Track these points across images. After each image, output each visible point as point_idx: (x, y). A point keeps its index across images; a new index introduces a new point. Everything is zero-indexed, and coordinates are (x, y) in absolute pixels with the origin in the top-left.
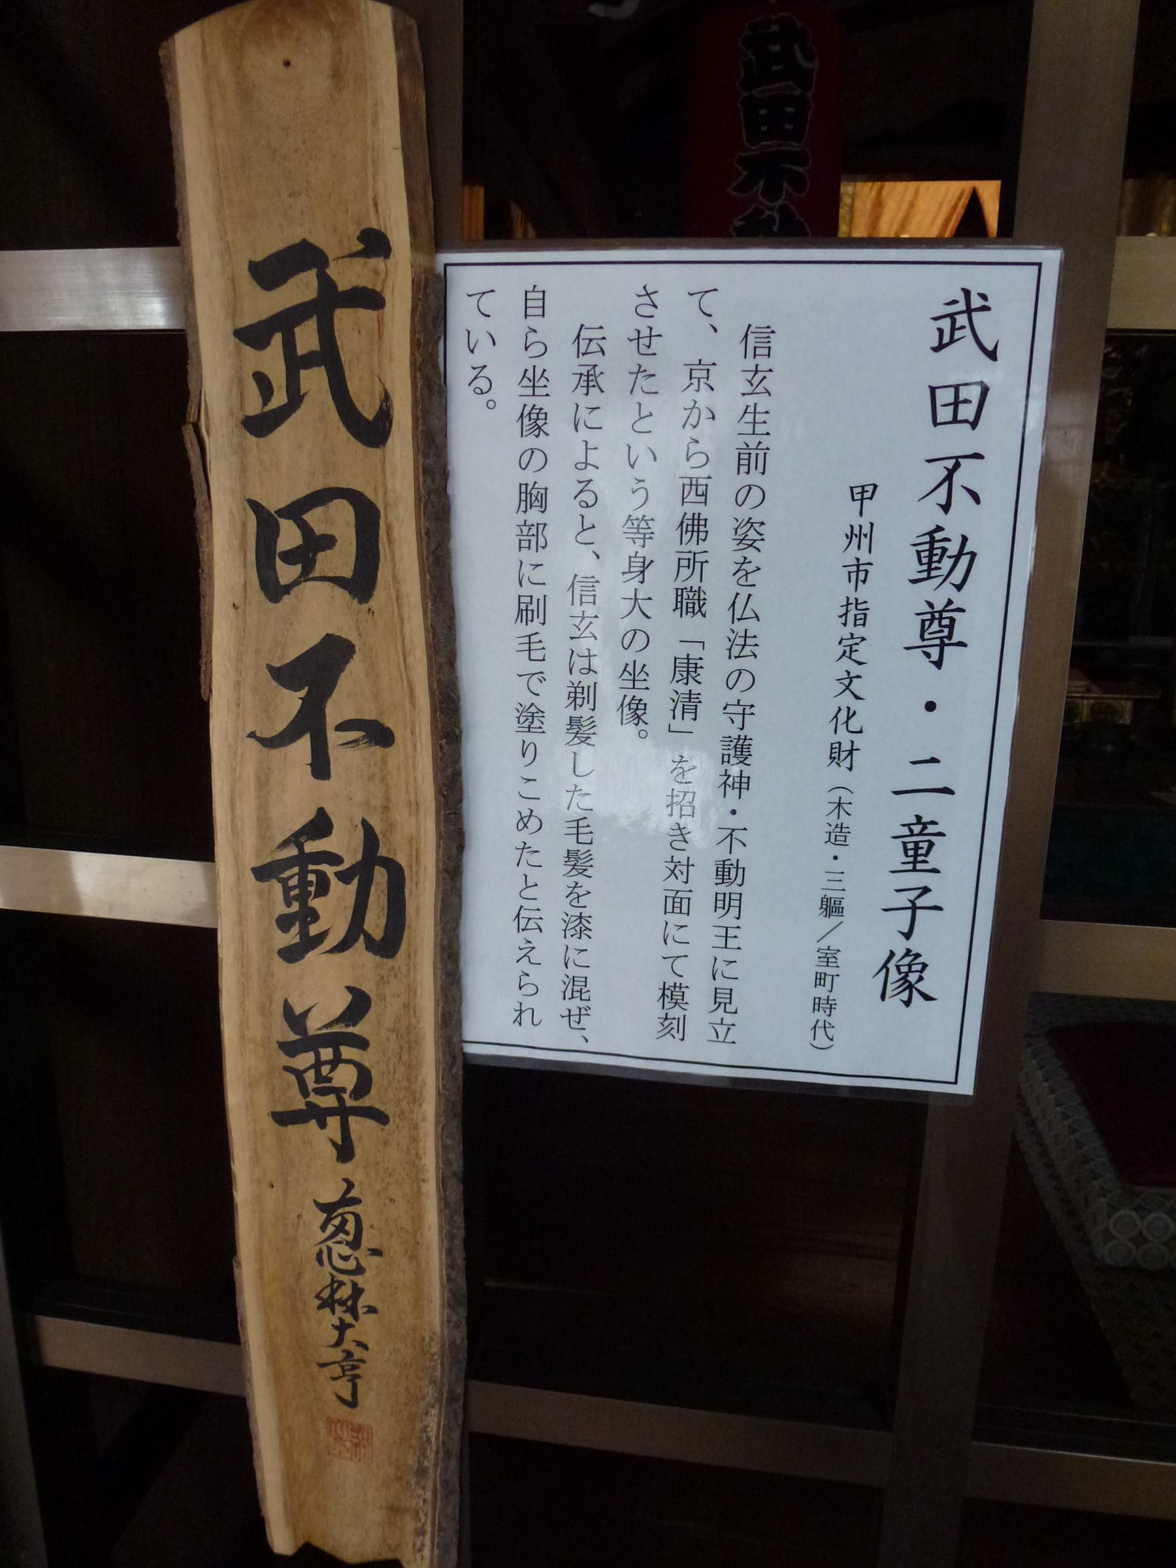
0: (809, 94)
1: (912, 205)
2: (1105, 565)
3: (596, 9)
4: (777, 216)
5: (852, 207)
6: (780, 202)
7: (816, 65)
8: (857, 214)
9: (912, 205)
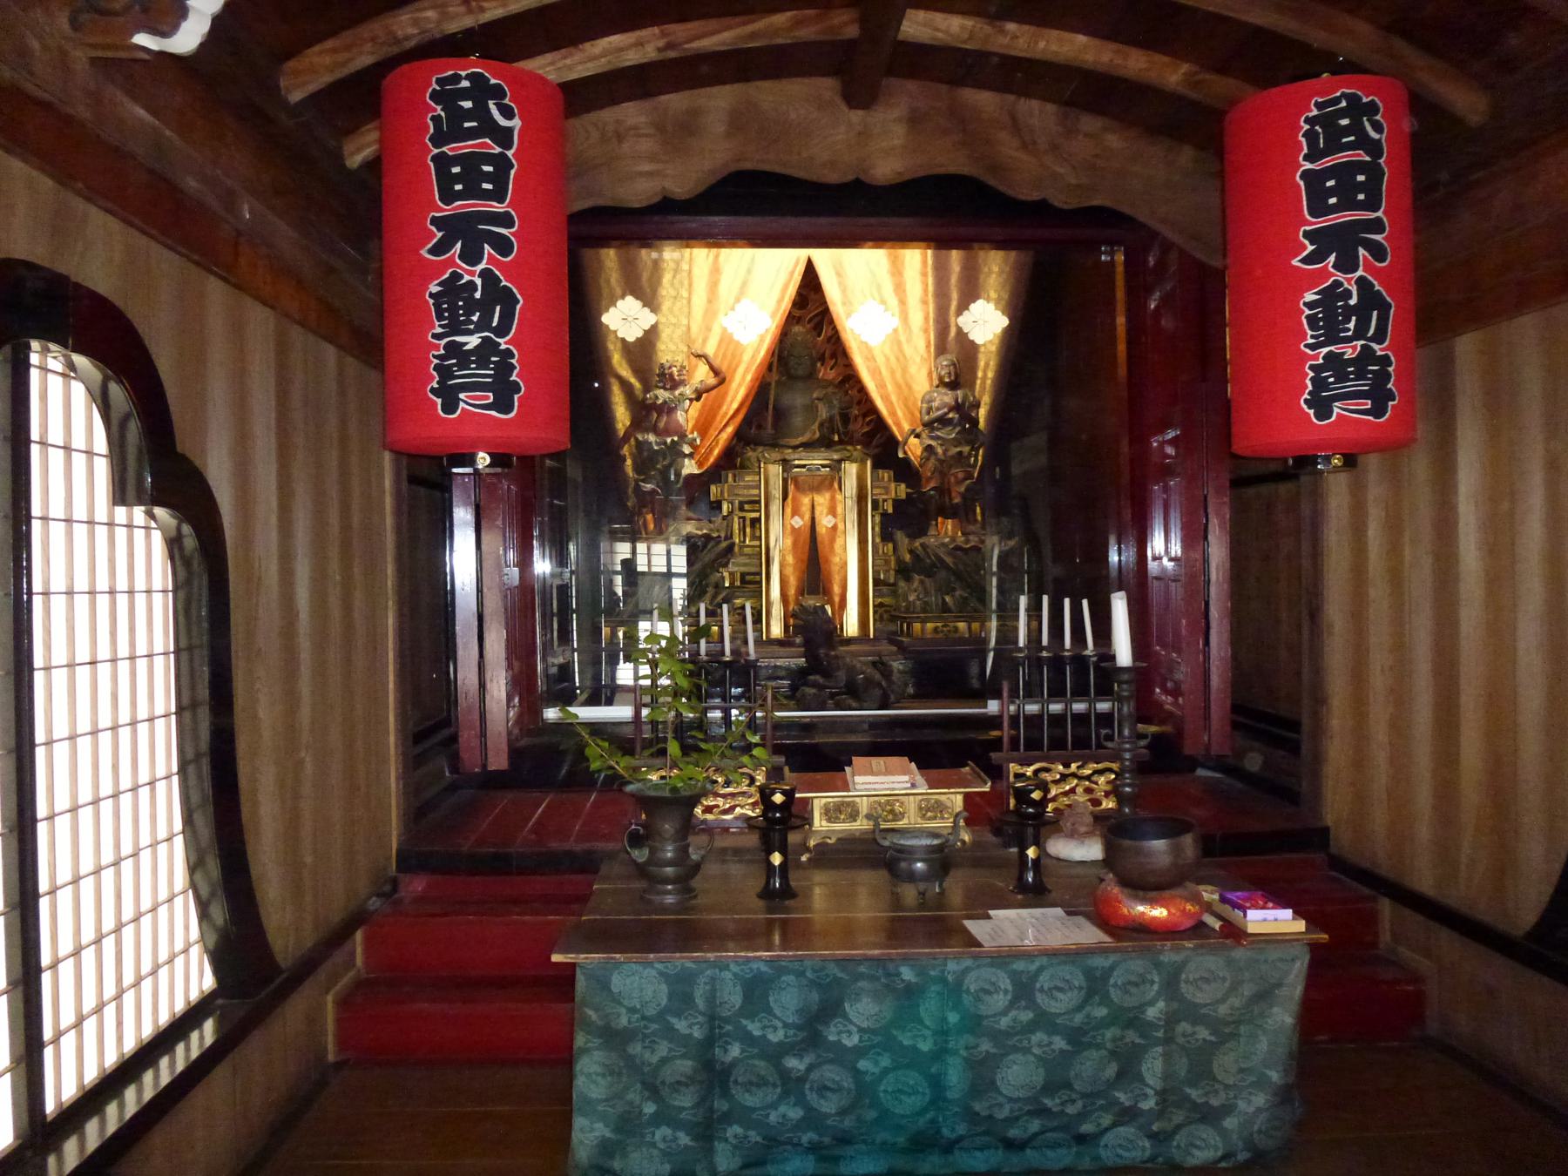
1: (749, 271)
2: (962, 625)
3: (142, 39)
4: (478, 282)
5: (690, 272)
7: (516, 123)
8: (695, 279)
9: (749, 271)
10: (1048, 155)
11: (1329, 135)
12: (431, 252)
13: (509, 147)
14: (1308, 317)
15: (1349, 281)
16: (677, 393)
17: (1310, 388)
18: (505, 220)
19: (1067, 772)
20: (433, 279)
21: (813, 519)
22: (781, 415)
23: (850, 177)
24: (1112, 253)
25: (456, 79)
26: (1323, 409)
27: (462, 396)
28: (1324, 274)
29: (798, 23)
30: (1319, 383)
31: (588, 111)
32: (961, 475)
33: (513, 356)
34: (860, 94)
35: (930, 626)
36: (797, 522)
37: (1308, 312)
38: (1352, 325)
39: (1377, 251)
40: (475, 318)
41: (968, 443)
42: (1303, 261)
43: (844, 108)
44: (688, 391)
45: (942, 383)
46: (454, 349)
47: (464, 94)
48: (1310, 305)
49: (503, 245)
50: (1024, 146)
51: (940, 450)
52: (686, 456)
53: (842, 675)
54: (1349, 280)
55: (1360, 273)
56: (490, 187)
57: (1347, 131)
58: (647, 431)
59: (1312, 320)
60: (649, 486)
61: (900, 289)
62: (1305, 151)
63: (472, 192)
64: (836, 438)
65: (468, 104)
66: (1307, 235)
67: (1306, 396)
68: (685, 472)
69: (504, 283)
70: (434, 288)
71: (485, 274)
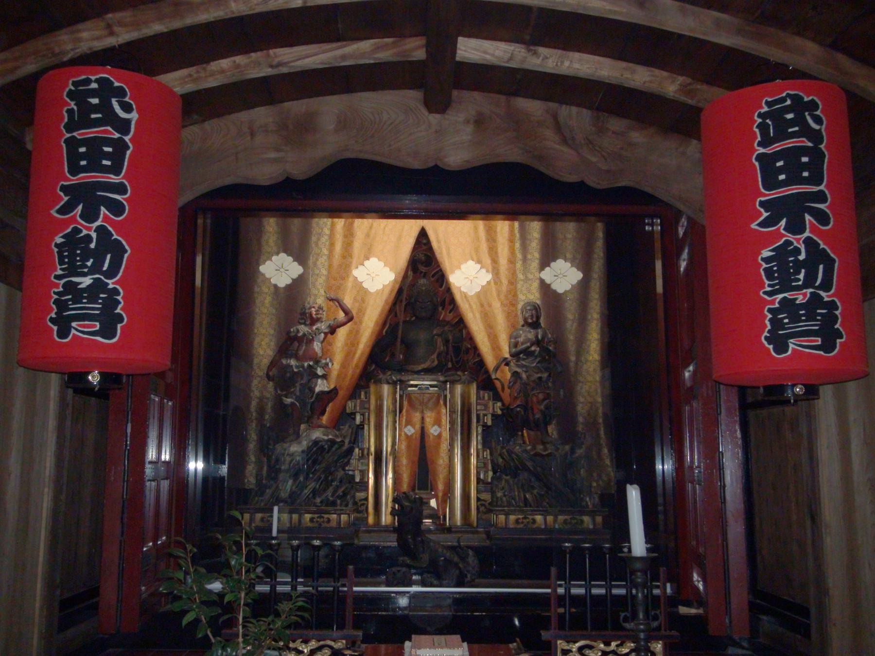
0: (822, 146)
2: (539, 518)
6: (98, 223)
7: (134, 116)
10: (572, 144)
11: (777, 125)
12: (58, 212)
13: (127, 133)
14: (765, 270)
15: (798, 241)
16: (314, 328)
17: (769, 327)
18: (120, 189)
19: (608, 649)
20: (56, 235)
21: (423, 429)
22: (409, 346)
23: (431, 164)
24: (652, 225)
25: (88, 81)
26: (781, 346)
27: (74, 324)
28: (778, 235)
29: (378, 48)
30: (776, 324)
31: (230, 113)
32: (541, 396)
33: (119, 294)
34: (438, 103)
35: (512, 518)
36: (410, 430)
37: (765, 265)
38: (801, 276)
39: (822, 217)
40: (89, 264)
41: (546, 369)
42: (759, 225)
43: (426, 113)
44: (323, 326)
45: (526, 323)
46: (71, 288)
47: (93, 93)
48: (767, 260)
49: (116, 208)
50: (564, 141)
51: (524, 376)
52: (318, 377)
53: (426, 557)
54: (798, 240)
55: (807, 234)
56: (108, 163)
57: (792, 123)
58: (291, 357)
59: (769, 273)
60: (289, 401)
61: (493, 251)
62: (759, 139)
63: (94, 166)
64: (450, 365)
65: (95, 101)
66: (762, 204)
67: (766, 334)
68: (317, 389)
69: (115, 237)
70: (59, 240)
71: (99, 229)
